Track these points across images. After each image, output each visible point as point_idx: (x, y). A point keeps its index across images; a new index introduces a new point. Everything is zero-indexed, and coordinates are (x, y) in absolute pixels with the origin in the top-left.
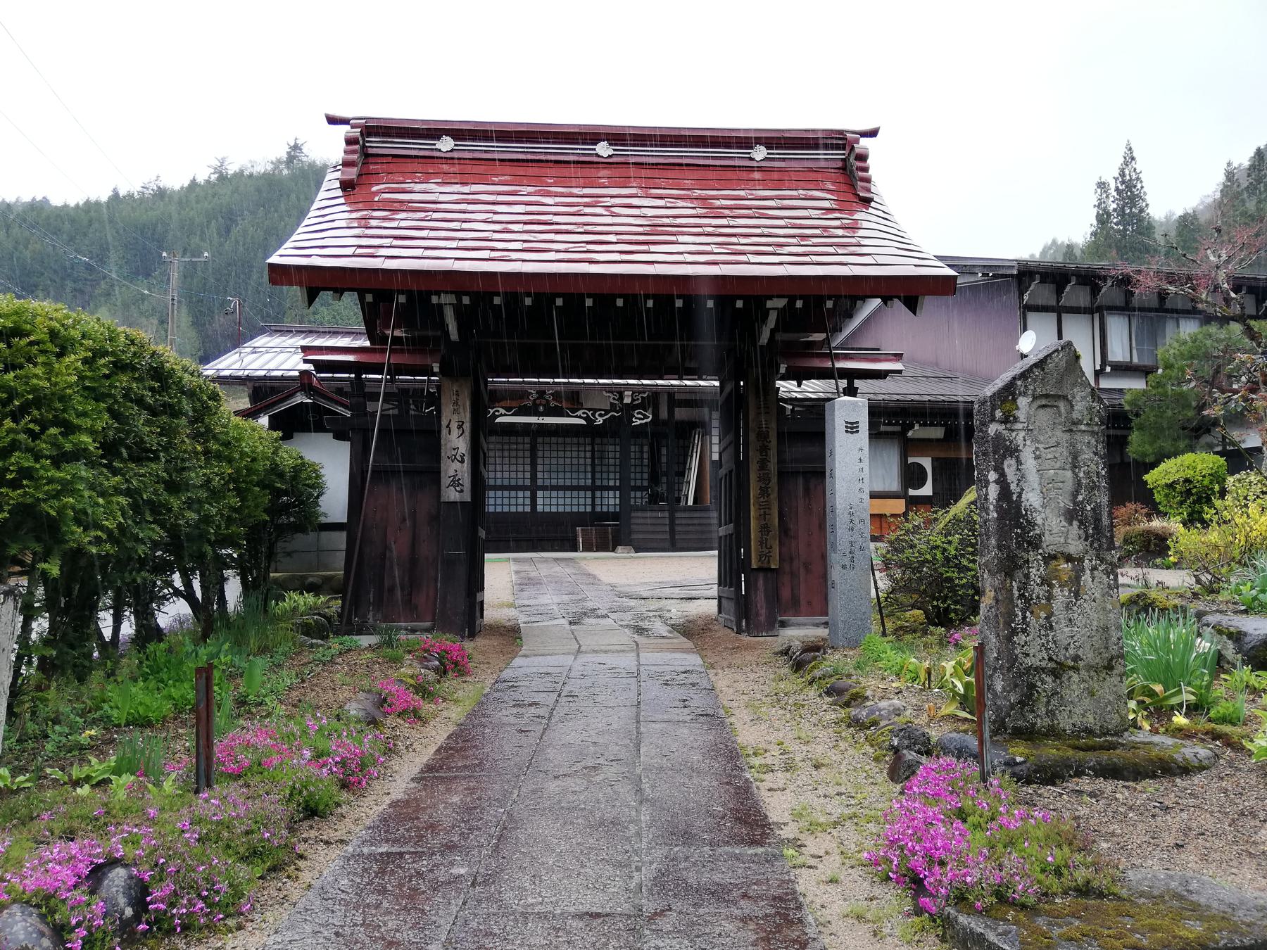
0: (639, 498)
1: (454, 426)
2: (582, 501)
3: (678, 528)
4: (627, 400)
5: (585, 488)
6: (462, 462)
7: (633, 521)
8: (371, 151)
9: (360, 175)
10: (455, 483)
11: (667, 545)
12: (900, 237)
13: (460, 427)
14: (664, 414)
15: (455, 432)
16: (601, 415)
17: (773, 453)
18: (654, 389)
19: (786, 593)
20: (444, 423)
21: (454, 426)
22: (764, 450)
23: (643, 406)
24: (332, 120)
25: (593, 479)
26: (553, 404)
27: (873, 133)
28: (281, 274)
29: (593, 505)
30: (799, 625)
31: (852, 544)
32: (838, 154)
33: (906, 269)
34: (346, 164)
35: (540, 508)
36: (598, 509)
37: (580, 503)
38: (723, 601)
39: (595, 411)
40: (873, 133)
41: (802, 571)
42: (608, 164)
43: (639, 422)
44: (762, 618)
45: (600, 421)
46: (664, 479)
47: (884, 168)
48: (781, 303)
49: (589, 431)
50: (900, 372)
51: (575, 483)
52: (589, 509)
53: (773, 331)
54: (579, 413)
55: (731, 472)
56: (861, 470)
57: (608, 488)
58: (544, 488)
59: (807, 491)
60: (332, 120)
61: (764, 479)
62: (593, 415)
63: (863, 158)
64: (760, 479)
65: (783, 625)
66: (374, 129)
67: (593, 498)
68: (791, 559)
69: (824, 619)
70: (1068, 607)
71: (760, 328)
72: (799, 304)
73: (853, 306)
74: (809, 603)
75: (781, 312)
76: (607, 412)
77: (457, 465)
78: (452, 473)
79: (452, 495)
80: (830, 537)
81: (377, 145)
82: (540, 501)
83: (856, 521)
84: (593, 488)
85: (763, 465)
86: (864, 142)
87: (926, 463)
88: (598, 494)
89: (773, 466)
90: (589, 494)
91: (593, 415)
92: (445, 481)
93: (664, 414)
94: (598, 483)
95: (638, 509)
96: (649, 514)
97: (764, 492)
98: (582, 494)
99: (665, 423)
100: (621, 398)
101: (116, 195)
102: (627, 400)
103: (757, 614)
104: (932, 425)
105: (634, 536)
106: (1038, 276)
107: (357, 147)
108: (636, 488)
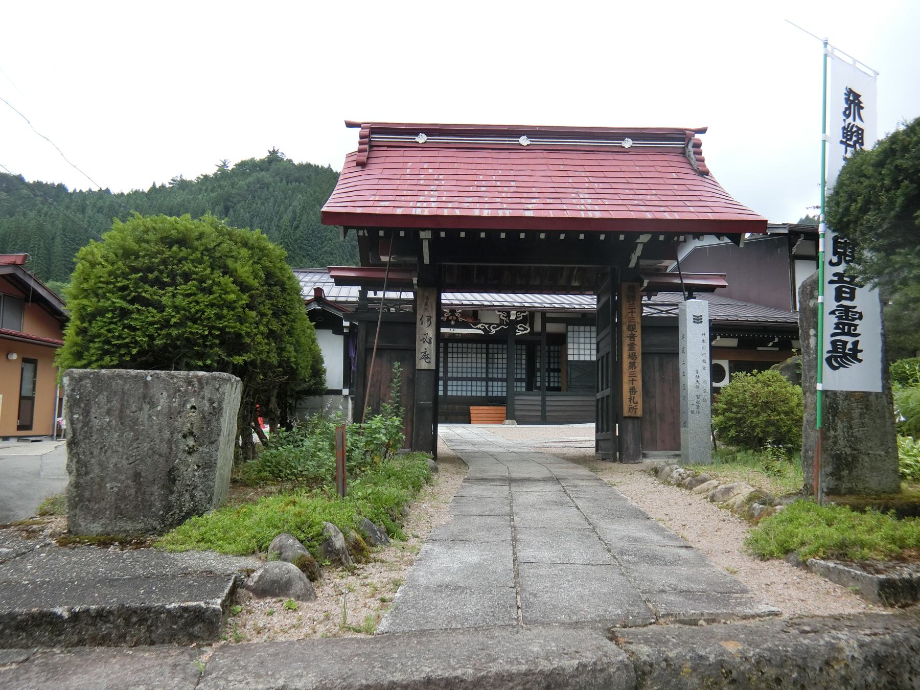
0: (521, 387)
1: (425, 319)
2: (479, 389)
3: (547, 408)
4: (513, 317)
5: (481, 379)
6: (430, 343)
7: (516, 402)
8: (373, 144)
9: (368, 158)
10: (426, 357)
11: (539, 419)
12: (725, 196)
13: (429, 320)
14: (538, 327)
15: (426, 323)
16: (494, 328)
17: (638, 341)
18: (532, 309)
19: (647, 435)
20: (419, 317)
21: (425, 319)
22: (632, 337)
23: (524, 321)
24: (350, 125)
25: (487, 373)
26: (460, 319)
27: (703, 131)
28: (330, 218)
29: (487, 391)
30: (655, 456)
31: (698, 397)
32: (679, 144)
33: (733, 216)
34: (360, 151)
35: (449, 393)
36: (490, 394)
37: (477, 390)
38: (600, 443)
39: (490, 324)
40: (703, 131)
41: (658, 420)
42: (528, 149)
43: (521, 333)
44: (631, 451)
45: (493, 331)
46: (538, 374)
47: (712, 153)
48: (645, 238)
49: (485, 340)
50: (724, 286)
51: (474, 375)
52: (484, 394)
53: (639, 258)
54: (479, 326)
55: (607, 354)
56: (704, 348)
57: (497, 380)
58: (453, 379)
59: (661, 366)
60: (350, 125)
61: (632, 356)
62: (489, 327)
63: (698, 145)
64: (630, 356)
65: (645, 456)
66: (377, 129)
67: (487, 386)
68: (651, 413)
69: (677, 452)
70: (862, 415)
71: (629, 255)
72: (662, 238)
73: (703, 234)
74: (663, 441)
75: (645, 245)
76: (498, 325)
77: (426, 345)
78: (423, 350)
79: (423, 365)
80: (682, 393)
81: (377, 138)
82: (449, 388)
83: (701, 382)
84: (487, 380)
85: (631, 347)
86: (697, 136)
87: (725, 364)
88: (490, 383)
89: (638, 349)
90: (484, 383)
91: (489, 327)
92: (419, 355)
93: (538, 327)
94: (490, 376)
95: (521, 394)
96: (526, 398)
97: (632, 365)
98: (479, 383)
99: (538, 334)
100: (509, 316)
101: (90, 190)
102: (513, 317)
103: (628, 449)
104: (729, 337)
105: (516, 413)
106: (802, 235)
107: (367, 140)
108: (518, 380)
